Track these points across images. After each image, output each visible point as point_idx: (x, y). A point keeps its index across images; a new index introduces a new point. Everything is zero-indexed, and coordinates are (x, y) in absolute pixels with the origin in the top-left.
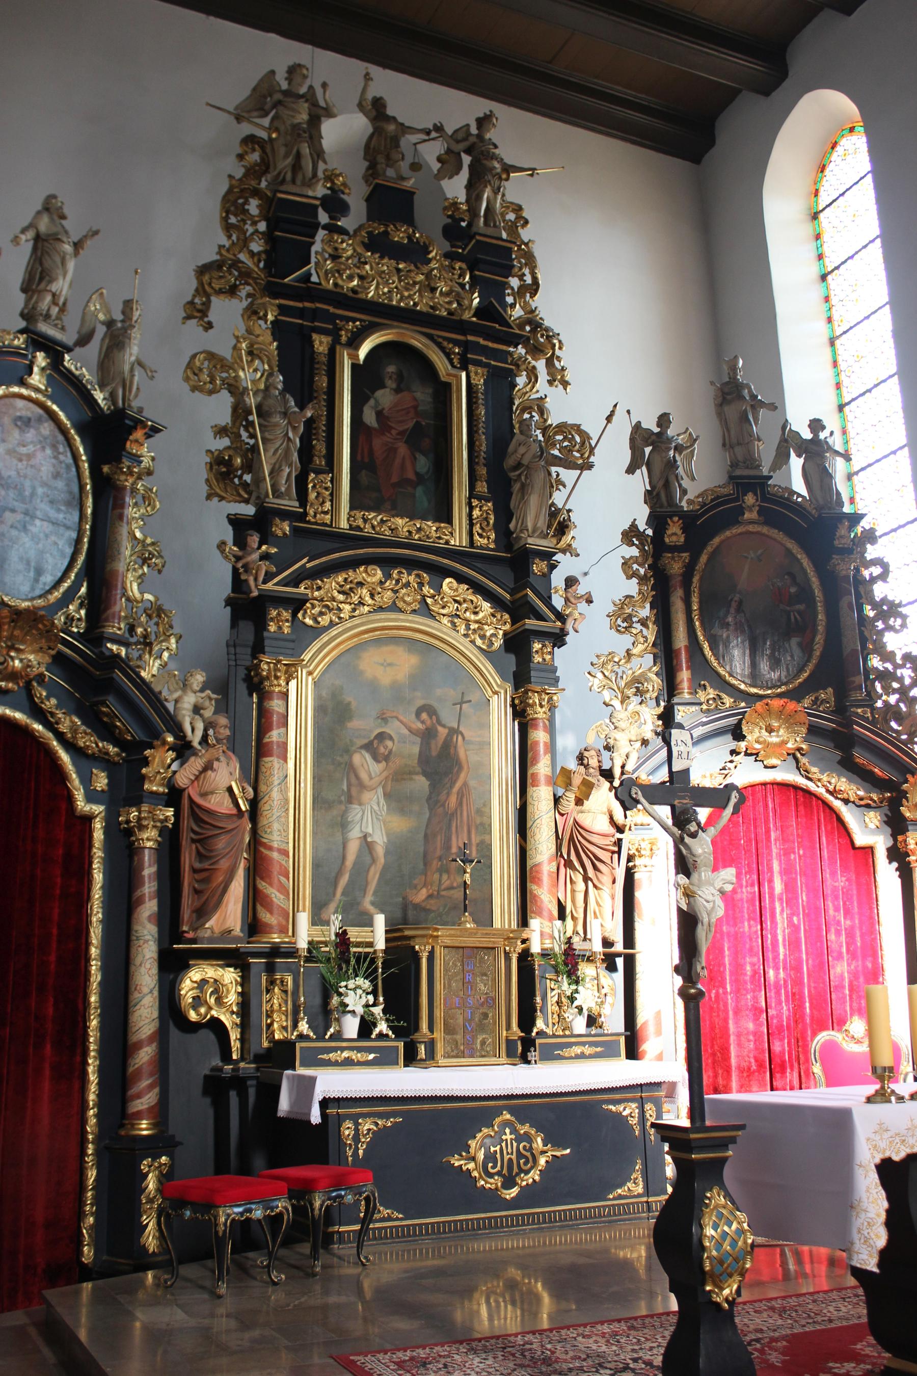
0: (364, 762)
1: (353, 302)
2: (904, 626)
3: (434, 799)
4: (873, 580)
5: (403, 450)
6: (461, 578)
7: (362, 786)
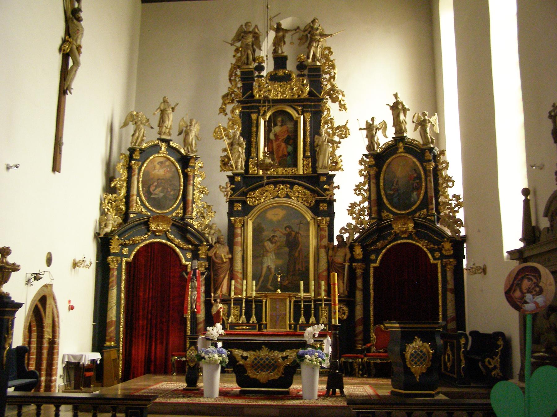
0: (268, 245)
1: (266, 100)
2: (453, 185)
3: (290, 254)
4: (443, 169)
5: (283, 145)
6: (300, 185)
7: (267, 251)
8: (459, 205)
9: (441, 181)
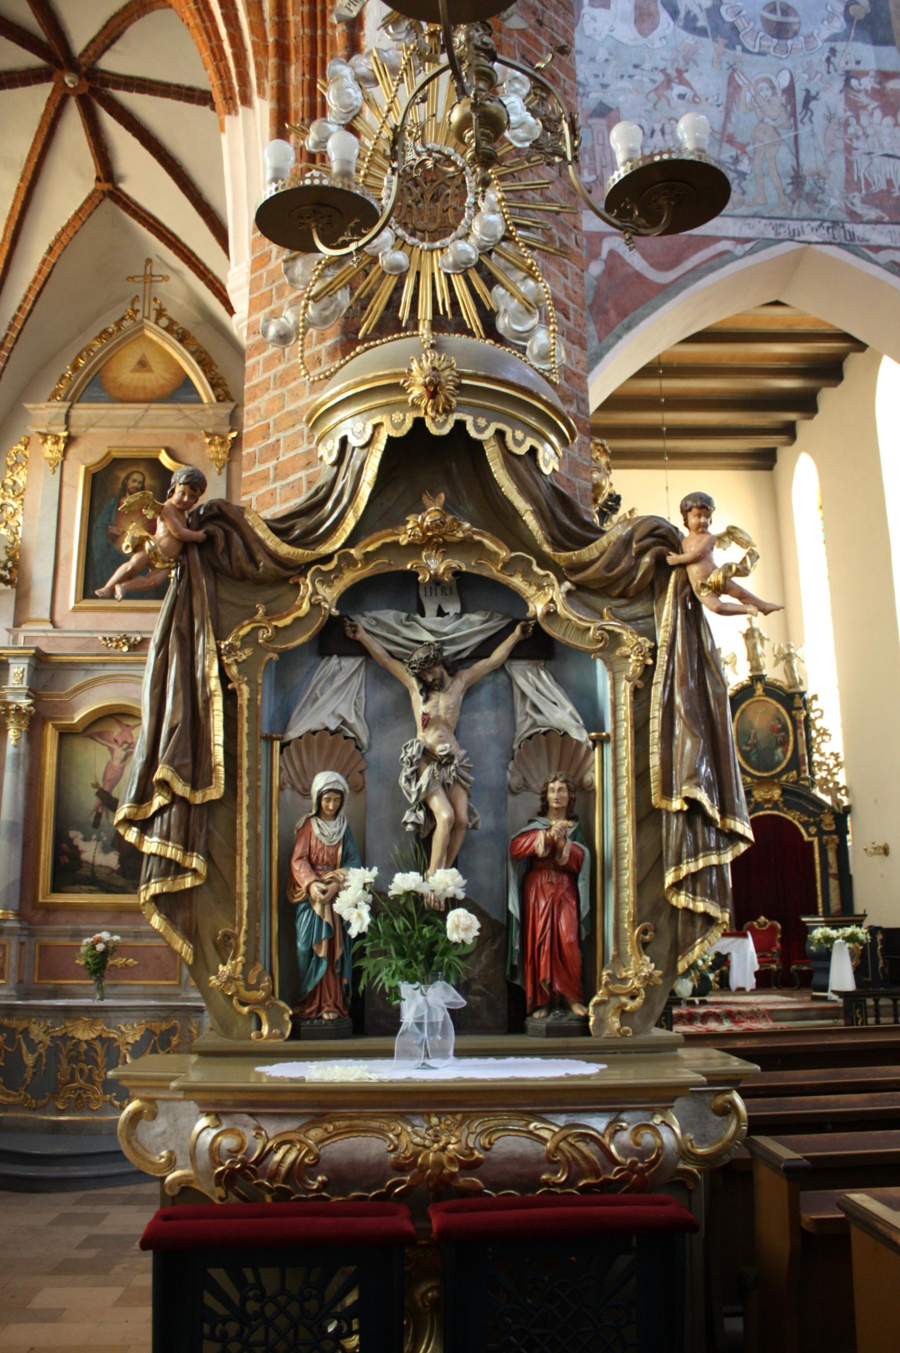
8: (838, 765)
9: (814, 734)
